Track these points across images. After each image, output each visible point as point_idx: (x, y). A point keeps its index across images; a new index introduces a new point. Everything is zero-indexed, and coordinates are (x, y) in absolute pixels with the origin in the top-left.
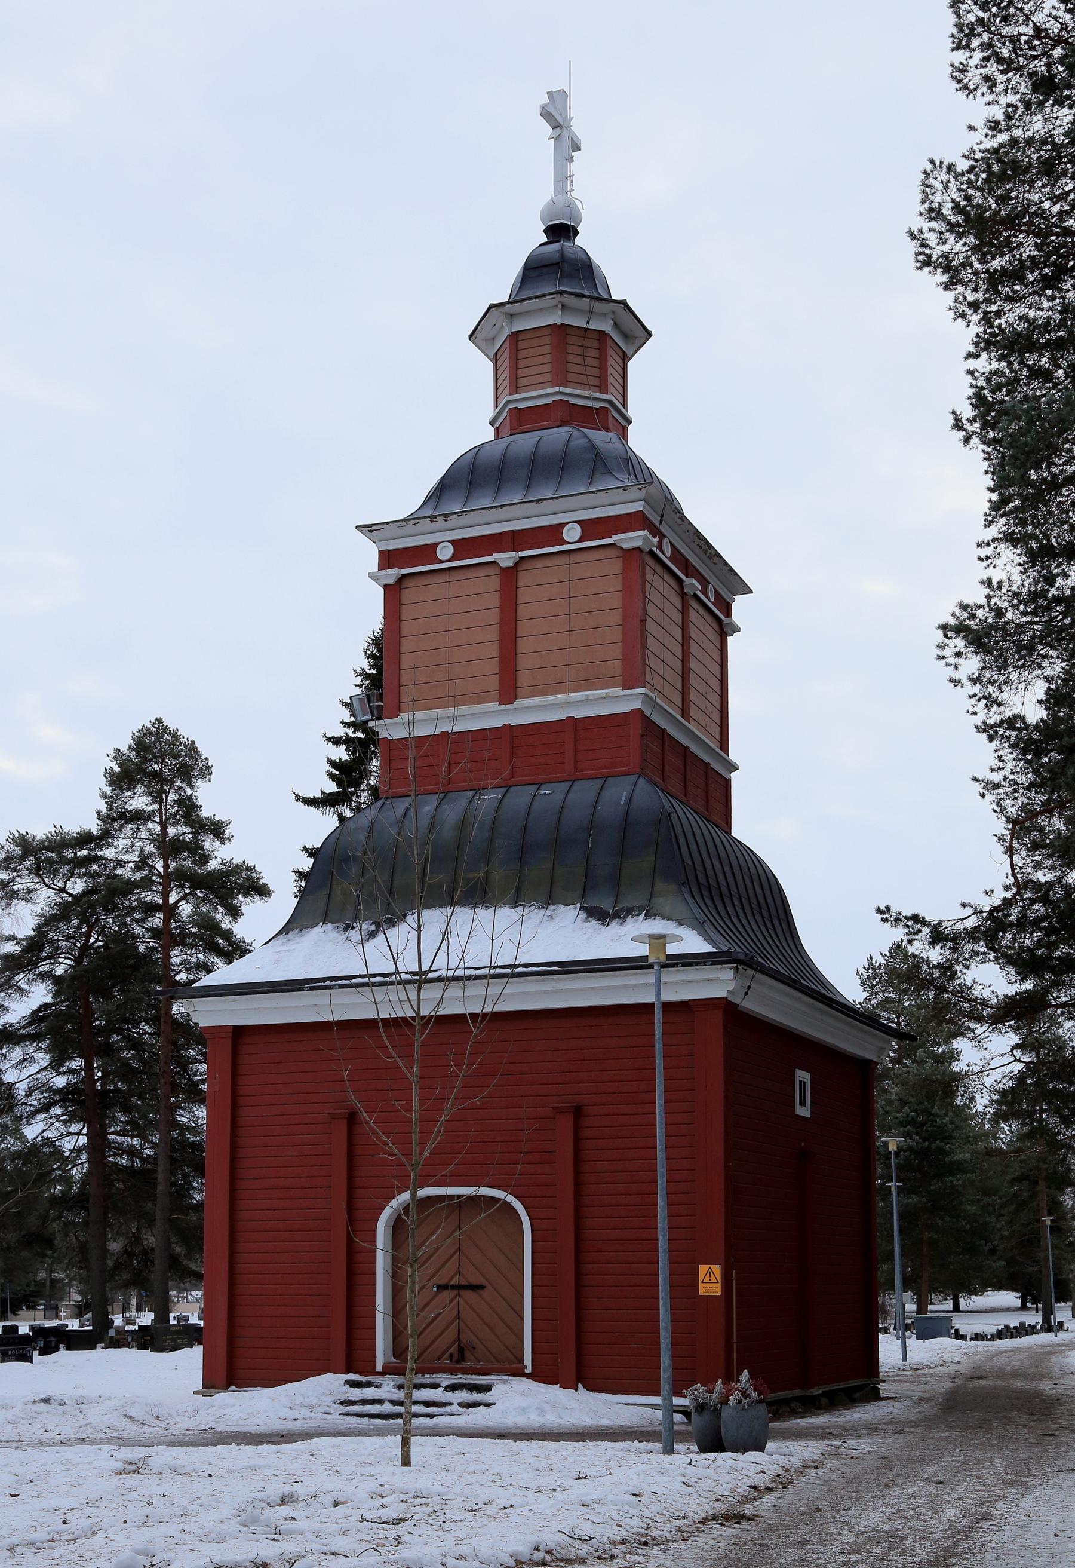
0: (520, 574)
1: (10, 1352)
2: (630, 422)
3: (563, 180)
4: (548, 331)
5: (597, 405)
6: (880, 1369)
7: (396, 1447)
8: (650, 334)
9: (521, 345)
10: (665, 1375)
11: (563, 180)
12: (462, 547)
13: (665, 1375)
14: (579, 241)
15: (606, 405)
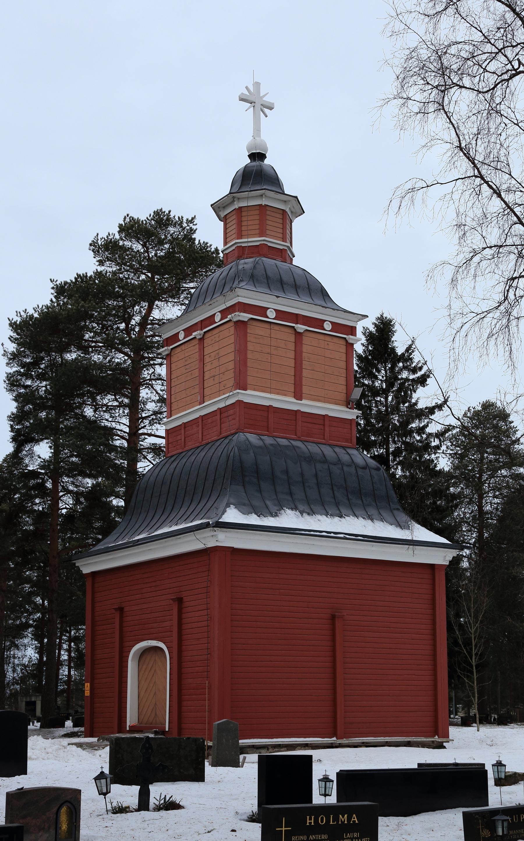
0: (205, 341)
1: (310, 821)
2: (294, 256)
3: (257, 129)
4: (258, 207)
5: (281, 247)
6: (150, 804)
7: (490, 779)
8: (304, 212)
9: (244, 214)
10: (478, 719)
11: (257, 129)
12: (280, 314)
13: (478, 719)
14: (267, 162)
15: (286, 248)
